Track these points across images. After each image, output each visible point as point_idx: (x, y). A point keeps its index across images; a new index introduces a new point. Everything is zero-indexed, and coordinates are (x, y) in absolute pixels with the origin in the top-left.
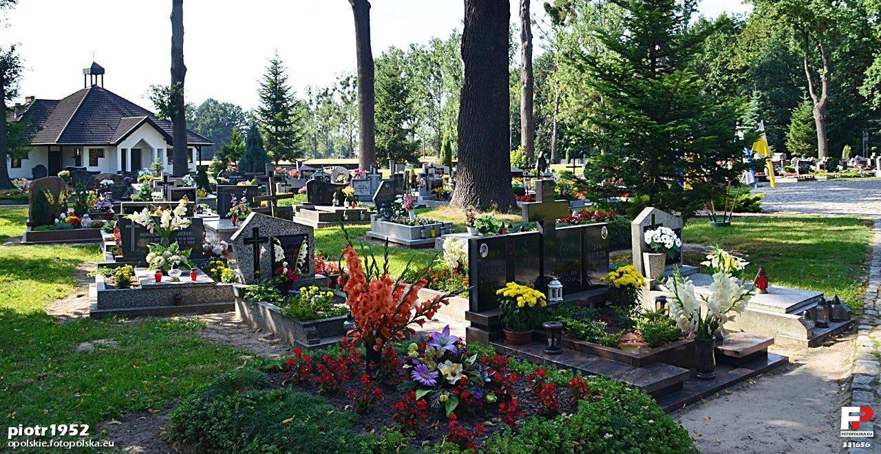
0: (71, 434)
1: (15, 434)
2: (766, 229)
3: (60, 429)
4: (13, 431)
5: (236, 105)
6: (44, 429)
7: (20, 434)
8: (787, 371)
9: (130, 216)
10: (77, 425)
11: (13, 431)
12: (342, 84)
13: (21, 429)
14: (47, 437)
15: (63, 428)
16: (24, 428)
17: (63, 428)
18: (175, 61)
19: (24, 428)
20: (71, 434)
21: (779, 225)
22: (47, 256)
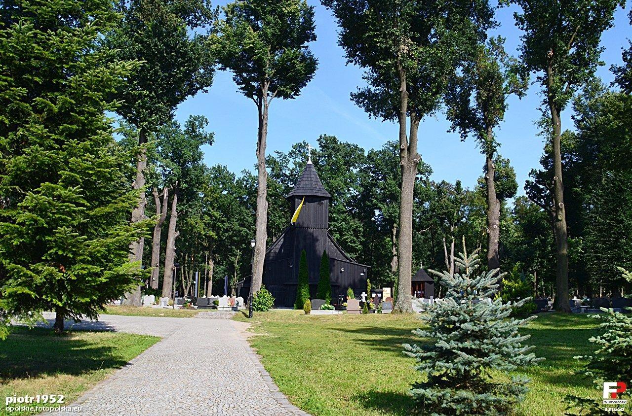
0: (51, 402)
1: (11, 402)
2: (156, 250)
3: (43, 398)
4: (9, 400)
5: (315, 32)
6: (32, 398)
7: (15, 402)
8: (426, 342)
9: (522, 178)
10: (55, 396)
11: (9, 400)
12: (352, 96)
13: (15, 398)
14: (34, 404)
15: (45, 397)
16: (17, 397)
17: (45, 397)
18: (30, 370)
19: (17, 397)
20: (51, 402)
21: (156, 250)
22: (157, 203)
